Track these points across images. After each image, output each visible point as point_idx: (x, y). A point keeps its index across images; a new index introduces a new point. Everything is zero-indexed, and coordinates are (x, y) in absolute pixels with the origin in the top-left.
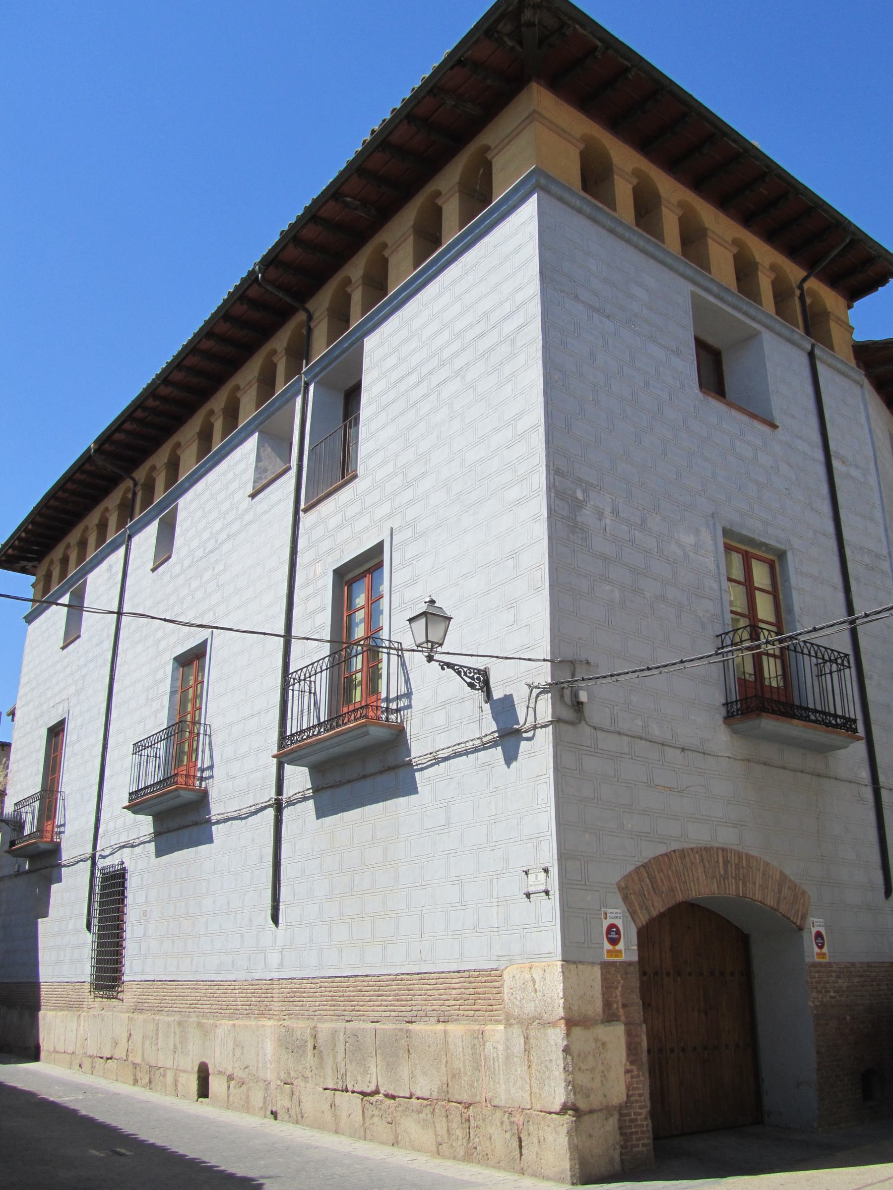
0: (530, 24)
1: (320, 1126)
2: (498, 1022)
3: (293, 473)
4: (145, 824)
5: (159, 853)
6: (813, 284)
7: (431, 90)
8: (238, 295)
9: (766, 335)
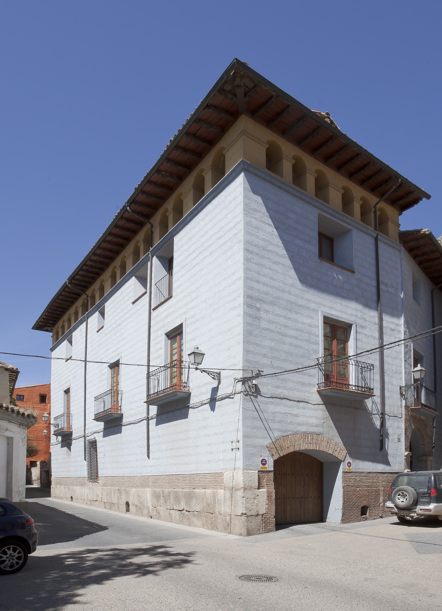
0: (239, 86)
1: (167, 521)
2: (222, 489)
3: (148, 294)
4: (101, 425)
5: (104, 436)
6: (382, 205)
7: (195, 120)
8: (120, 217)
9: (355, 232)
